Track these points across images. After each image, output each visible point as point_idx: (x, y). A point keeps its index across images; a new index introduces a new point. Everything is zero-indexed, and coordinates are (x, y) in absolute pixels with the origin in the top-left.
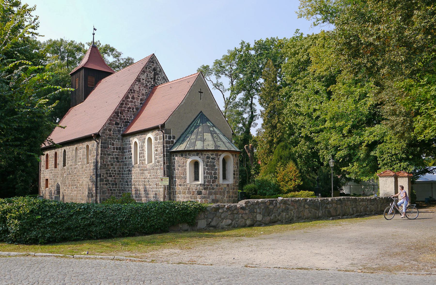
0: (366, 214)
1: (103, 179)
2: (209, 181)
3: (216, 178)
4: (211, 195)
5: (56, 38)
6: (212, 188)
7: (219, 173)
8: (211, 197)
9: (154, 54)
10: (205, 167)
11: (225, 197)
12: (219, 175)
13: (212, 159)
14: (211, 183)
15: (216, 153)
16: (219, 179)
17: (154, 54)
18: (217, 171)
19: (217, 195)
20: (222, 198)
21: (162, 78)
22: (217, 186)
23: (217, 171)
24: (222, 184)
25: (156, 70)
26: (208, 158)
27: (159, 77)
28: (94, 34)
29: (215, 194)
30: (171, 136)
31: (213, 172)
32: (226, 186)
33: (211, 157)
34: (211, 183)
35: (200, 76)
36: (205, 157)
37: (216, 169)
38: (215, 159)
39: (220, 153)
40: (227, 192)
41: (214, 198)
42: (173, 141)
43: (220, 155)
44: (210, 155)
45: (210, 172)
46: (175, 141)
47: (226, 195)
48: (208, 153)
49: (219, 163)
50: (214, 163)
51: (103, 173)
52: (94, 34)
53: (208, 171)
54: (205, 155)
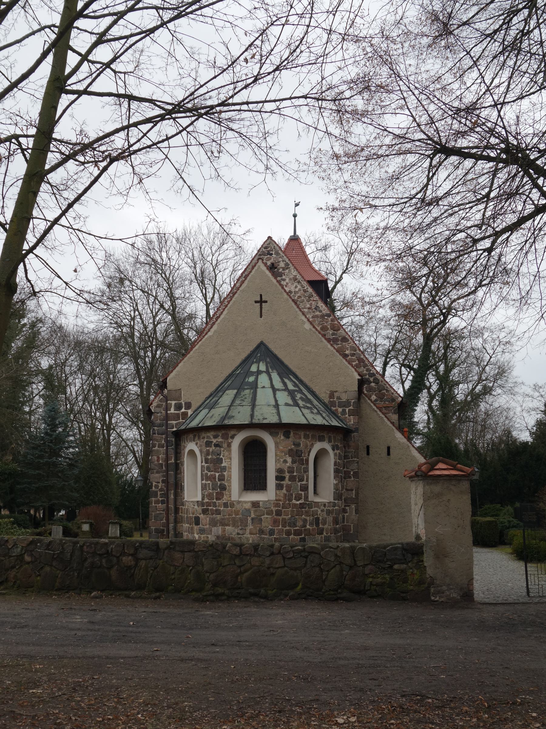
0: (256, 595)
1: (157, 492)
2: (210, 496)
3: (223, 488)
4: (215, 525)
5: (288, 237)
6: (216, 510)
7: (230, 476)
8: (214, 529)
9: (270, 238)
10: (204, 464)
11: (248, 531)
12: (229, 481)
13: (216, 445)
14: (215, 500)
15: (223, 432)
16: (230, 491)
17: (270, 238)
18: (225, 473)
19: (227, 528)
20: (238, 534)
21: (290, 279)
22: (226, 505)
23: (225, 473)
24: (239, 502)
25: (276, 268)
26: (208, 444)
27: (284, 280)
28: (295, 216)
29: (223, 524)
30: (181, 404)
31: (217, 474)
32: (247, 506)
33: (214, 441)
34: (215, 500)
35: (259, 266)
36: (203, 442)
37: (224, 468)
38: (220, 447)
39: (232, 433)
40: (253, 519)
41: (220, 532)
42: (185, 415)
43: (233, 437)
44: (212, 437)
45: (212, 475)
46: (190, 412)
47: (250, 527)
48: (209, 434)
49: (230, 454)
50: (219, 454)
51: (156, 480)
52: (295, 216)
53: (209, 474)
54: (204, 438)
